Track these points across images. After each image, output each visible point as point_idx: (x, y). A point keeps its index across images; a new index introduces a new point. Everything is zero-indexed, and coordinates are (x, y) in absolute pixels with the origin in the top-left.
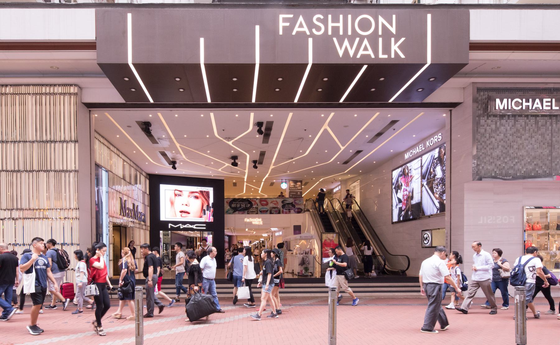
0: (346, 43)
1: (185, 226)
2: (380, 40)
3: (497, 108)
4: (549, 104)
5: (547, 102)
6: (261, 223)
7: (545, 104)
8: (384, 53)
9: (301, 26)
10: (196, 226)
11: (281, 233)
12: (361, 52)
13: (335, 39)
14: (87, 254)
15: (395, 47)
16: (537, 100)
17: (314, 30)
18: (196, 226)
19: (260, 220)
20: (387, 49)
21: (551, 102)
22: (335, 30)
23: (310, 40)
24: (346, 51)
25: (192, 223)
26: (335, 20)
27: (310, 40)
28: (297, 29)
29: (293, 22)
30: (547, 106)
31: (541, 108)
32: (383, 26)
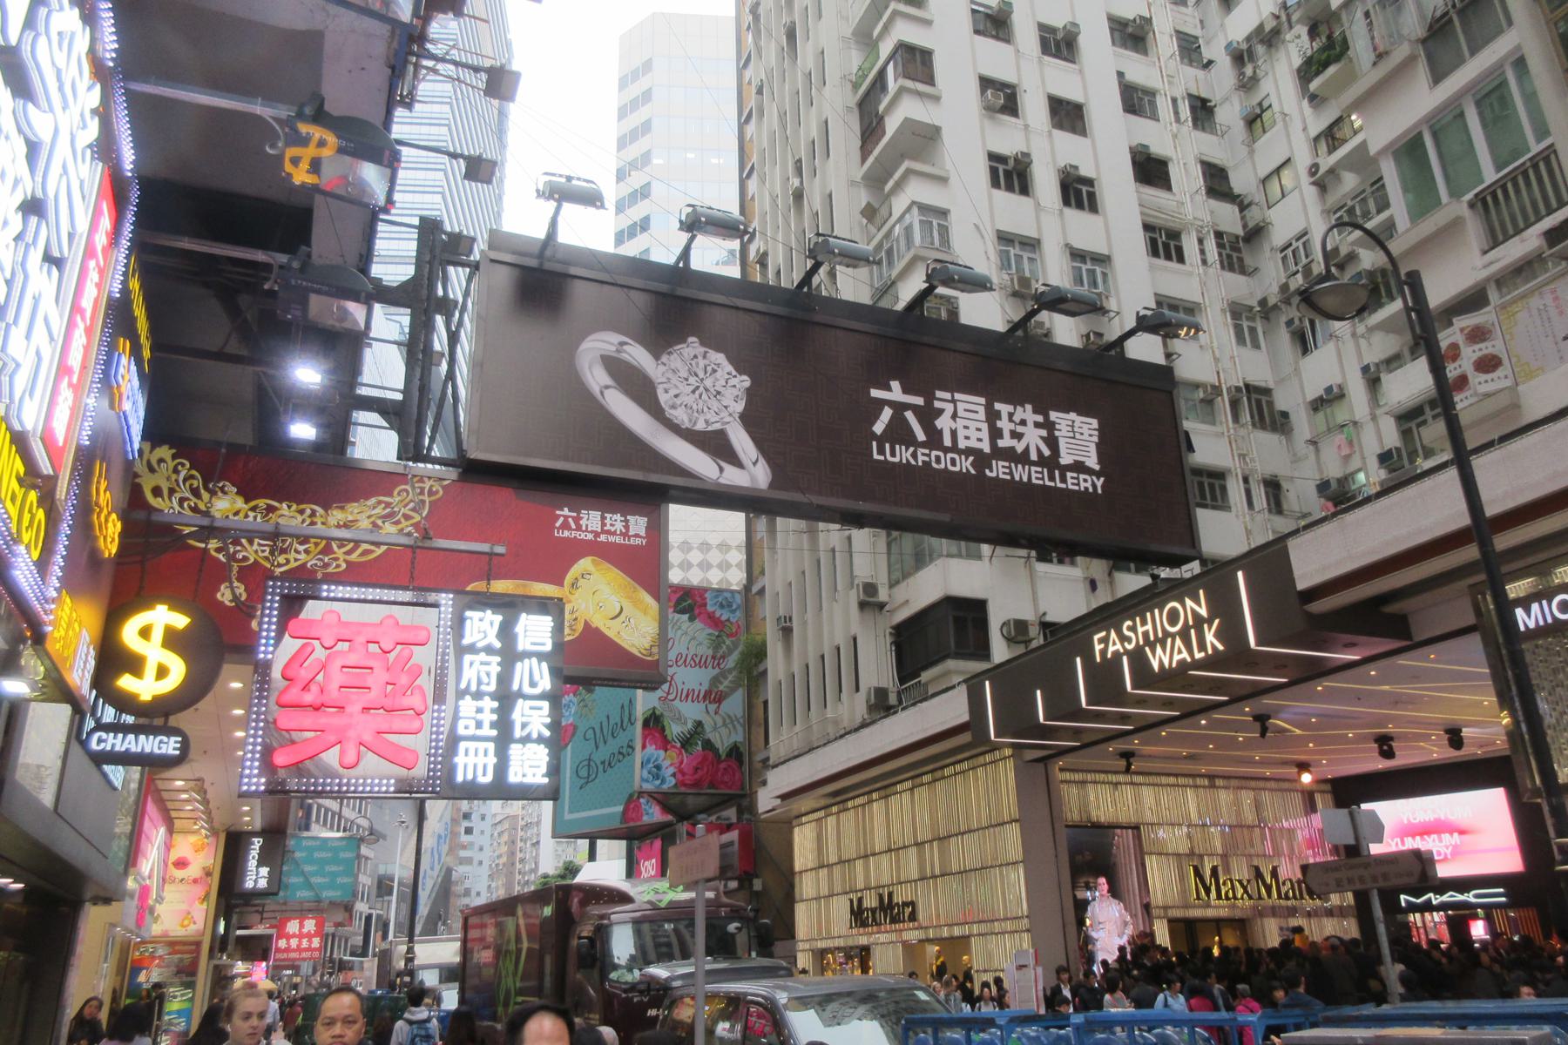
0: (1159, 650)
1: (1445, 898)
3: (1522, 628)
6: (314, 299)
9: (1115, 646)
10: (1476, 896)
11: (1216, 952)
12: (1177, 657)
14: (93, 1002)
15: (1210, 637)
18: (1476, 896)
19: (1373, 852)
20: (1202, 647)
22: (1146, 634)
23: (1125, 659)
24: (1161, 662)
25: (857, 826)
26: (1144, 623)
27: (1125, 659)
28: (1111, 649)
29: (1105, 640)
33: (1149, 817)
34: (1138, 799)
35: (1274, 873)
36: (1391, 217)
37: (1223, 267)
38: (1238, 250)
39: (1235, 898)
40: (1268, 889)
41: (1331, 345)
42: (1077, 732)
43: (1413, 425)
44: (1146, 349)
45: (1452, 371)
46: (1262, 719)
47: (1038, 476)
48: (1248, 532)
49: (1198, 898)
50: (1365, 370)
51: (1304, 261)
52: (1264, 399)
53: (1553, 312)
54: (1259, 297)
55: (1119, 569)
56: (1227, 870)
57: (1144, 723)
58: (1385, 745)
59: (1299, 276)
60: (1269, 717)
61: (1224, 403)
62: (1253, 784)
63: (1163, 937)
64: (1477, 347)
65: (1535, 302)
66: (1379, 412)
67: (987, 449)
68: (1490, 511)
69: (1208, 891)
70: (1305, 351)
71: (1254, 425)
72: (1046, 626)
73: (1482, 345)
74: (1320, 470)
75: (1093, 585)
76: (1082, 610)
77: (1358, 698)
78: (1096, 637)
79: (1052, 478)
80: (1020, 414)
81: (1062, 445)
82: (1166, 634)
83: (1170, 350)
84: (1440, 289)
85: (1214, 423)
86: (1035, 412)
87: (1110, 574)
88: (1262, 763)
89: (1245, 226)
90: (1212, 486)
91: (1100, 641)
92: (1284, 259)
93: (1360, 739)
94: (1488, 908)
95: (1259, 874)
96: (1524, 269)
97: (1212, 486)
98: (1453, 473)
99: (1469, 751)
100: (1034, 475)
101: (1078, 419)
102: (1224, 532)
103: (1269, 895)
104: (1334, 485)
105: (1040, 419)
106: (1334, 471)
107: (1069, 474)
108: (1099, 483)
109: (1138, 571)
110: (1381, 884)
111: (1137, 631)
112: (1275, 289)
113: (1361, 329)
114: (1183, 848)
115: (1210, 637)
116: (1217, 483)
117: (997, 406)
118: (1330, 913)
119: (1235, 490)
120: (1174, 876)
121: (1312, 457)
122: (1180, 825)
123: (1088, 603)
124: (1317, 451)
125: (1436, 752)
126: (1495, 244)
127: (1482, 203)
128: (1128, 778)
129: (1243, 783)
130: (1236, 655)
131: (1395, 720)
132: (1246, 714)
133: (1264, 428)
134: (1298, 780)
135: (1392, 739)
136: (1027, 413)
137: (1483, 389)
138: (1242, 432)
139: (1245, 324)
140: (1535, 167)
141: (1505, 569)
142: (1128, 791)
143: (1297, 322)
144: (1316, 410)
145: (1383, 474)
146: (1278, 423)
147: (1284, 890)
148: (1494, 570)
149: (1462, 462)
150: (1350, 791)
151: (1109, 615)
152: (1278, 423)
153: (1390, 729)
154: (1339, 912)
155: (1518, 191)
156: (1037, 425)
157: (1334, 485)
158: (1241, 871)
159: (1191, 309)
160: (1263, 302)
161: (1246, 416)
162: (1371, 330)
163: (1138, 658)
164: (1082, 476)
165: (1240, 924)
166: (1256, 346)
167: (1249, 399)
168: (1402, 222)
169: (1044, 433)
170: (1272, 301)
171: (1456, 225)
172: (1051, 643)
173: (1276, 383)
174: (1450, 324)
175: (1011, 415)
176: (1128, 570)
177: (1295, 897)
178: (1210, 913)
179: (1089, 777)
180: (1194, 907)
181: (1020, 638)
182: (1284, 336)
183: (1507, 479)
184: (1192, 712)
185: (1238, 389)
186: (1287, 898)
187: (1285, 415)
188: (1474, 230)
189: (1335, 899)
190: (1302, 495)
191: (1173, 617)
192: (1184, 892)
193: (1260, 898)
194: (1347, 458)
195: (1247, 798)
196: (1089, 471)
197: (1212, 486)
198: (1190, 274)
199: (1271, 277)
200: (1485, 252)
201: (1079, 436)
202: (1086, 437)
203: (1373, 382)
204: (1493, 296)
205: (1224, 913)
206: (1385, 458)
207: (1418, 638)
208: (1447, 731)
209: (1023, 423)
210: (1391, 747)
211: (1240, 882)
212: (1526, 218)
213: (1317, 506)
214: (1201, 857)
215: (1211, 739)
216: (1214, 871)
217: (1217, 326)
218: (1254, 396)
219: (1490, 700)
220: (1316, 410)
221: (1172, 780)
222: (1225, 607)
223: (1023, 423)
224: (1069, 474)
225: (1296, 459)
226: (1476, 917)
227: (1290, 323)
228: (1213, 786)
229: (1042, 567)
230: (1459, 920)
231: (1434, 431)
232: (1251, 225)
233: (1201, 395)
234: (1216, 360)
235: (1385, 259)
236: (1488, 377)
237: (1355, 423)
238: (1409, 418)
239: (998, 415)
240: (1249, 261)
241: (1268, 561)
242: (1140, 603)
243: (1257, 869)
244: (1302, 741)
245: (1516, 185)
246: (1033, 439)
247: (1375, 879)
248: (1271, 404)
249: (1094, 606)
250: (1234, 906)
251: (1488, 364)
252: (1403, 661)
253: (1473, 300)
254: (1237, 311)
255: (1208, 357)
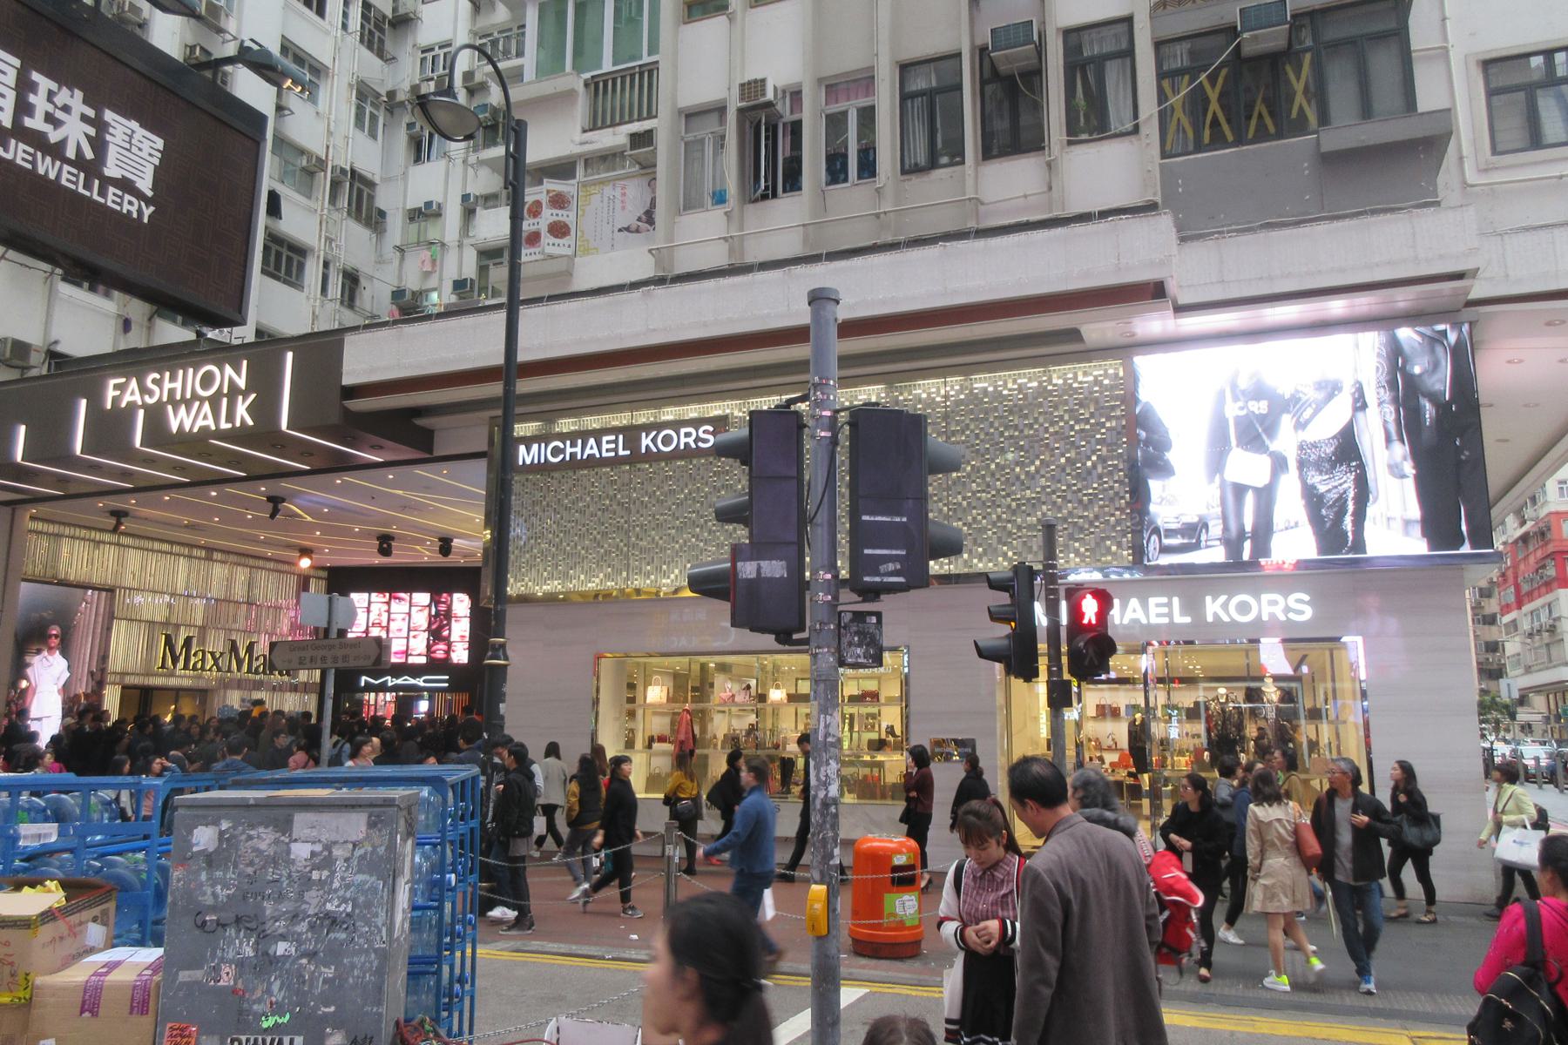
2: (225, 400)
4: (1165, 610)
5: (1158, 605)
7: (605, 446)
8: (227, 421)
9: (132, 395)
11: (1361, 929)
12: (200, 423)
13: (170, 408)
16: (592, 441)
17: (147, 398)
20: (230, 417)
21: (1169, 605)
22: (172, 392)
23: (141, 413)
26: (173, 379)
30: (1158, 615)
31: (1144, 621)
32: (231, 380)
33: (128, 581)
34: (121, 562)
35: (250, 649)
36: (521, 67)
37: (362, 41)
38: (382, 31)
39: (203, 668)
40: (240, 663)
41: (443, 163)
42: (62, 481)
43: (490, 263)
44: (248, 88)
45: (528, 225)
46: (275, 501)
47: (69, 178)
48: (315, 317)
49: (163, 667)
50: (465, 198)
51: (441, 71)
52: (366, 191)
53: (618, 205)
54: (390, 88)
55: (161, 316)
56: (202, 641)
57: (142, 484)
58: (385, 543)
59: (432, 84)
60: (283, 500)
61: (324, 181)
62: (251, 562)
63: (111, 701)
64: (555, 211)
65: (608, 190)
66: (466, 241)
67: (8, 124)
68: (522, 357)
69: (175, 660)
70: (418, 159)
71: (349, 213)
72: (53, 356)
73: (560, 212)
74: (400, 278)
75: (127, 325)
76: (107, 348)
77: (373, 497)
78: (112, 382)
79: (88, 186)
80: (63, 97)
81: (112, 154)
82: (195, 397)
83: (283, 103)
84: (539, 149)
85: (309, 197)
86: (85, 102)
87: (150, 319)
88: (267, 543)
89: (395, 10)
90: (289, 259)
91: (116, 387)
92: (423, 60)
93: (362, 534)
94: (431, 691)
95: (234, 648)
96: (607, 158)
97: (287, 260)
98: (502, 316)
99: (455, 560)
100: (65, 175)
101: (141, 133)
102: (276, 306)
103: (239, 669)
104: (408, 296)
105: (91, 113)
106: (412, 283)
107: (111, 190)
108: (148, 211)
109: (184, 324)
110: (340, 665)
111: (162, 385)
112: (406, 86)
113: (472, 159)
114: (159, 617)
115: (241, 410)
116: (296, 258)
117: (35, 76)
118: (294, 688)
119: (313, 271)
120: (142, 643)
121: (396, 262)
122: (162, 593)
123: (115, 342)
124: (402, 259)
125: (426, 555)
126: (594, 128)
127: (597, 86)
128: (114, 538)
129: (243, 560)
130: (263, 433)
131: (395, 520)
132: (261, 494)
133: (358, 218)
134: (293, 564)
135: (393, 539)
136: (74, 99)
137: (549, 250)
138: (336, 216)
139: (368, 109)
140: (641, 74)
141: (518, 410)
142: (111, 553)
143: (418, 127)
144: (412, 219)
145: (453, 299)
146: (374, 219)
147: (255, 665)
148: (508, 409)
149: (512, 309)
150: (343, 580)
151: (133, 361)
152: (374, 219)
153: (394, 530)
154: (305, 688)
155: (623, 89)
156: (84, 118)
157: (408, 296)
158: (216, 643)
159: (318, 70)
160: (391, 94)
161: (343, 202)
162: (481, 163)
163: (156, 416)
164: (127, 197)
165: (202, 694)
166: (373, 135)
167: (351, 186)
168: (529, 74)
169: (92, 131)
170: (401, 97)
171: (570, 95)
172: (57, 376)
173: (383, 180)
174: (540, 183)
175: (51, 95)
176: (174, 321)
177: (264, 672)
178: (172, 682)
179: (67, 531)
180: (156, 675)
181: (16, 362)
182: (401, 138)
183: (547, 333)
184: (204, 481)
185: (343, 171)
186: (257, 672)
187: (382, 214)
188: (581, 109)
189: (303, 676)
190: (376, 296)
191: (207, 380)
192: (149, 660)
193: (229, 671)
194: (427, 275)
195: (241, 575)
196: (139, 195)
197: (289, 259)
198: (327, 33)
199: (405, 75)
200: (585, 131)
201: (136, 152)
202: (144, 154)
203: (469, 213)
204: (580, 170)
205: (186, 683)
206: (459, 285)
207: (438, 452)
208: (441, 540)
209: (66, 109)
210: (390, 546)
211: (212, 654)
212: (622, 116)
213: (386, 310)
214: (177, 626)
215: (218, 512)
216: (188, 642)
217: (337, 98)
218: (357, 184)
219: (479, 518)
220: (412, 219)
221: (166, 547)
222: (264, 385)
223: (66, 109)
224: (111, 190)
225: (380, 261)
226: (422, 698)
227: (410, 126)
228: (209, 559)
229: (65, 289)
230: (405, 704)
231: (499, 274)
232: (401, 11)
233: (304, 163)
234: (330, 133)
235: (503, 101)
236: (557, 241)
237: (443, 245)
238: (488, 255)
239: (33, 87)
240: (389, 46)
241: (321, 350)
242: (170, 358)
243: (234, 643)
244: (311, 527)
245: (623, 83)
246: (74, 133)
247: (335, 659)
248: (371, 198)
249: (122, 347)
250: (200, 677)
251: (559, 230)
252: (419, 471)
253: (562, 169)
254: (364, 93)
255: (321, 127)
